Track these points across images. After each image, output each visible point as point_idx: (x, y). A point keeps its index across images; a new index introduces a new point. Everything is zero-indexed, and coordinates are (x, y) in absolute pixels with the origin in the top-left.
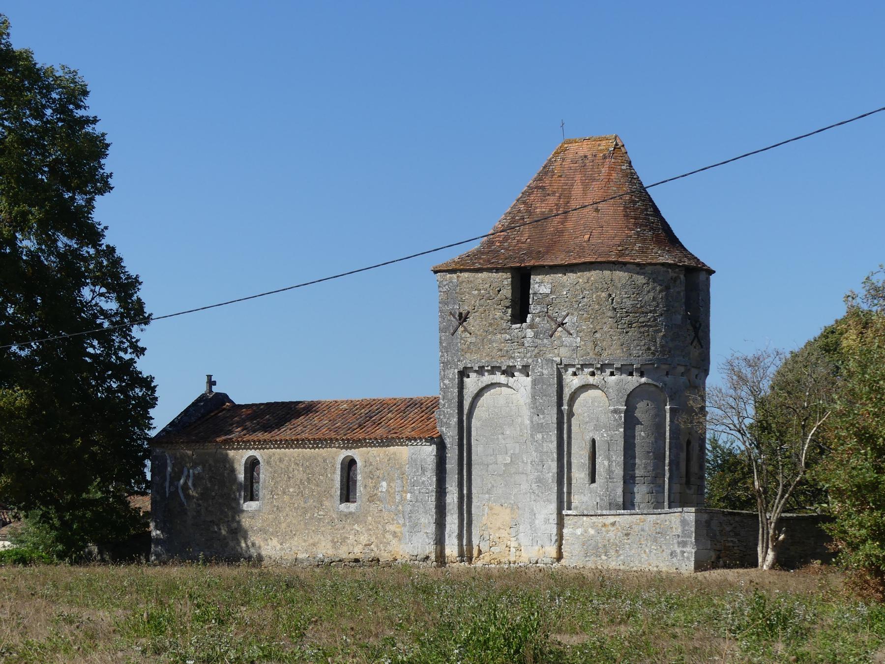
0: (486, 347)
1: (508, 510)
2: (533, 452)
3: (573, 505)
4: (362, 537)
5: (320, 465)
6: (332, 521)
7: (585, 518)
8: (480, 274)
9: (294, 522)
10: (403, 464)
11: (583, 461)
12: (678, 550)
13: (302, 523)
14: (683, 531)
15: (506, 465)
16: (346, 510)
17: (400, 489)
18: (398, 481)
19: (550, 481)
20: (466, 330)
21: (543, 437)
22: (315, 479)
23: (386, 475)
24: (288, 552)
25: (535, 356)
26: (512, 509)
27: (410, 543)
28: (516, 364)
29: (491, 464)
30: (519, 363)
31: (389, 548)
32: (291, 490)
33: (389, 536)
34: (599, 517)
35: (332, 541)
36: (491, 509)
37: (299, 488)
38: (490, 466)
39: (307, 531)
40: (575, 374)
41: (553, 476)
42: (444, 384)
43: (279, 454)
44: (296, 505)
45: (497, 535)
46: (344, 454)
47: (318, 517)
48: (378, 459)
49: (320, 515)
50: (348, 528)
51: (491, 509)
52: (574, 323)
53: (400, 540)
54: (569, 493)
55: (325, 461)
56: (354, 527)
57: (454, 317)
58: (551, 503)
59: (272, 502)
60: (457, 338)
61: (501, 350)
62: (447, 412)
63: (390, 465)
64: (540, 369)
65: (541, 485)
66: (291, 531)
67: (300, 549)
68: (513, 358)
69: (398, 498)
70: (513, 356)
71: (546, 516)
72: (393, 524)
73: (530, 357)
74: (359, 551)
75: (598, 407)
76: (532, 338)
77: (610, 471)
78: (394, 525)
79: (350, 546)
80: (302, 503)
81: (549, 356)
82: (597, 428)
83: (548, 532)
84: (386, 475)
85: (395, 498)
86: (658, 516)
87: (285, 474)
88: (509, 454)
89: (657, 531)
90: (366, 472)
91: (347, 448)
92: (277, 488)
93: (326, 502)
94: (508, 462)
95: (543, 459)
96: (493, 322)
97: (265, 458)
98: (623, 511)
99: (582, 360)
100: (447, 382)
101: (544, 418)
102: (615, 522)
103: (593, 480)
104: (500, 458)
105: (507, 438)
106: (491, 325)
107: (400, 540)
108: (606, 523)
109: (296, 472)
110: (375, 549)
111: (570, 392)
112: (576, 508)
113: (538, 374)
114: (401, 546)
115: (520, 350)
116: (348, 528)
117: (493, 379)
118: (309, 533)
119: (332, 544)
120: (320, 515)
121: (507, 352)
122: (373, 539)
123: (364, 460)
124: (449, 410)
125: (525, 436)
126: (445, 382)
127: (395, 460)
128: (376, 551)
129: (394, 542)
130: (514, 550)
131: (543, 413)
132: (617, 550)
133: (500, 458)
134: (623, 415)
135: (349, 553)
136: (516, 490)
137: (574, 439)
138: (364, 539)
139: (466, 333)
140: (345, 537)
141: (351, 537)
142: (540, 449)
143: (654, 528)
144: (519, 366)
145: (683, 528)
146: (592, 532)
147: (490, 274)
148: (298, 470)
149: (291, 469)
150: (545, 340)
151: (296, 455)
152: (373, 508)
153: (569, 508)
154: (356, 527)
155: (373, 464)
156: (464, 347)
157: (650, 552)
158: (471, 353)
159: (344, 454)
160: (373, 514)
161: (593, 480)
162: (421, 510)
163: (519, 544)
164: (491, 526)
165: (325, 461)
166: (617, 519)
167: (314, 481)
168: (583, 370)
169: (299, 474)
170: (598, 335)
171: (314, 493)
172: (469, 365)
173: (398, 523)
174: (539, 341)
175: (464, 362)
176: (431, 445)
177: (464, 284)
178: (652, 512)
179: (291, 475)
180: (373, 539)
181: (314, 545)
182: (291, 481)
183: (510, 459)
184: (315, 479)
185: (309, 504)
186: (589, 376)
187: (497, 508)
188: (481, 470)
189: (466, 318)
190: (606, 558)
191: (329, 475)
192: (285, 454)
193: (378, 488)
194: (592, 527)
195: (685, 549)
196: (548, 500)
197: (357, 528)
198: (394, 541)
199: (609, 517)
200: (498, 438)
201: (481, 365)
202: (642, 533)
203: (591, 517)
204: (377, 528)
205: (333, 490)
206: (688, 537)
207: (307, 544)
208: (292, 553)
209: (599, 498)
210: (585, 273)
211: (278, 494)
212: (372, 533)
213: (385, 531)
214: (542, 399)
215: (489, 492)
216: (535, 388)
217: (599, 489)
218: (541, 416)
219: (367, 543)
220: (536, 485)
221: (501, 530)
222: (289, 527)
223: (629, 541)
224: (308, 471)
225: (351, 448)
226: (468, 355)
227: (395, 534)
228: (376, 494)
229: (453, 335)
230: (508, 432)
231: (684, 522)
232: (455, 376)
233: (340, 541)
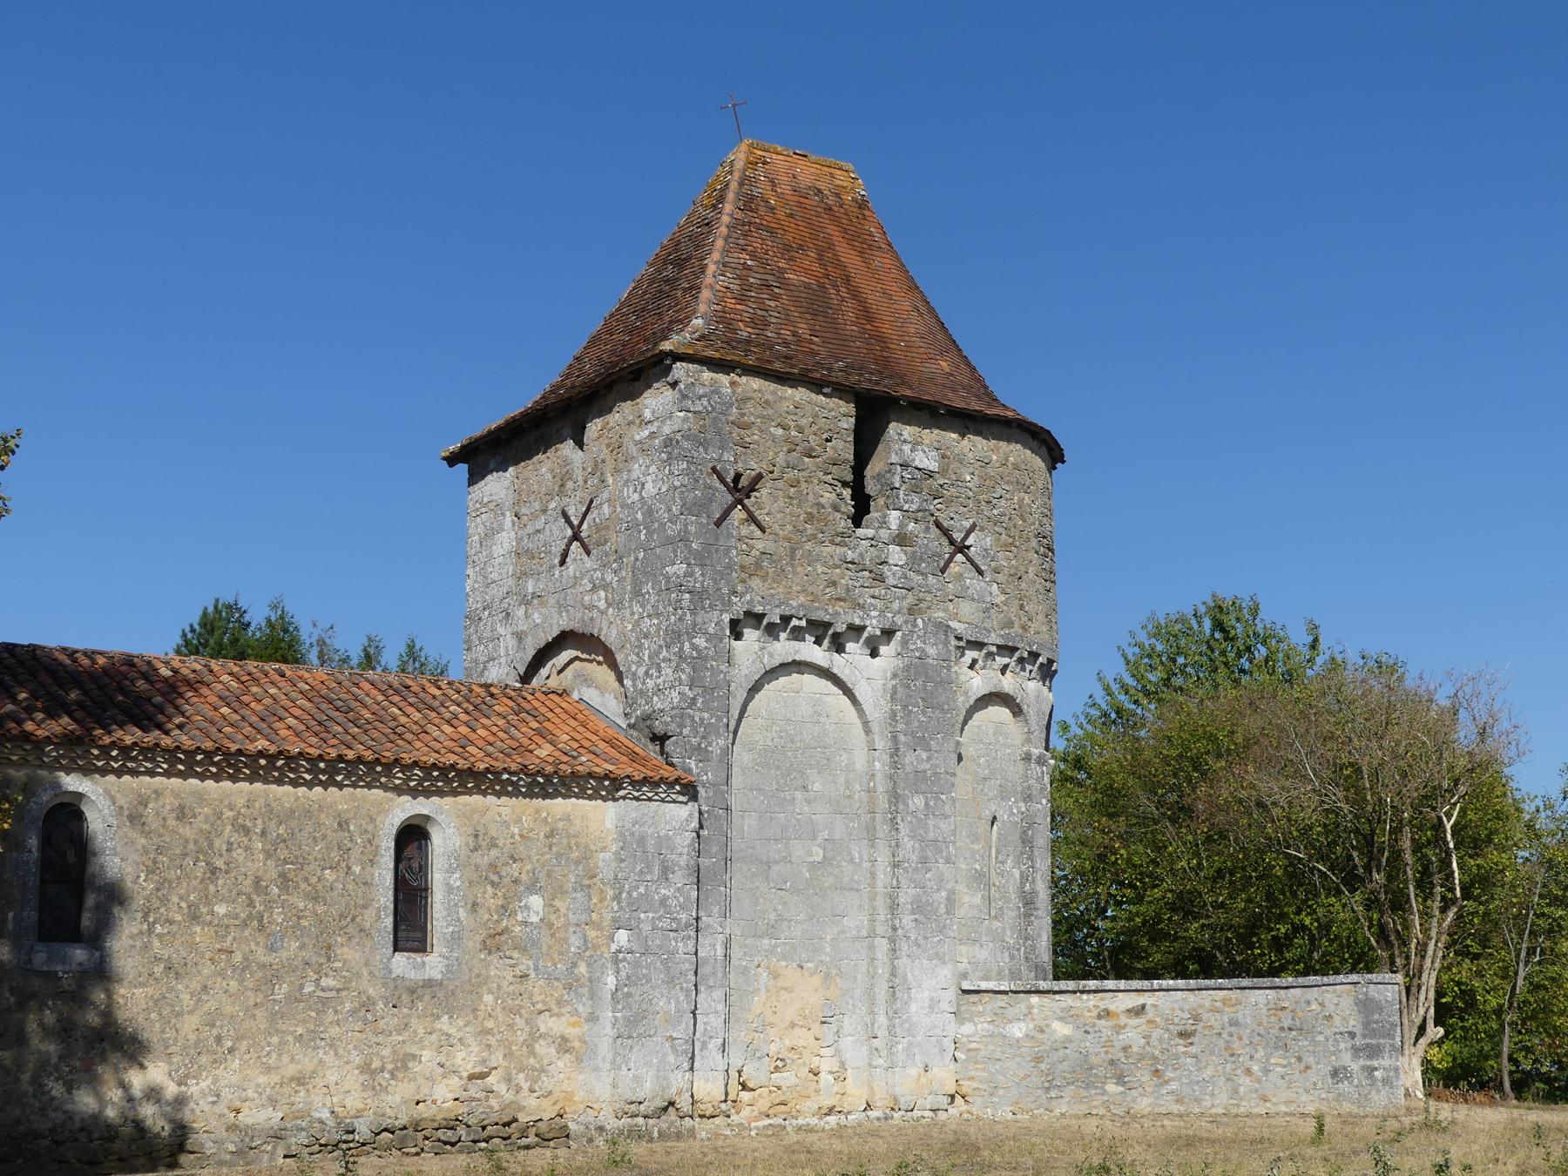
0: (799, 569)
1: (817, 980)
2: (906, 839)
4: (461, 1055)
5: (324, 837)
6: (367, 1005)
7: (1035, 999)
8: (790, 391)
9: (228, 1010)
10: (593, 848)
11: (978, 867)
12: (1355, 1067)
13: (260, 1013)
14: (1366, 1025)
15: (813, 866)
16: (412, 975)
17: (583, 917)
18: (579, 895)
20: (752, 519)
21: (927, 804)
22: (306, 880)
23: (542, 876)
24: (207, 1108)
25: (911, 611)
26: (827, 977)
27: (624, 1068)
28: (868, 623)
29: (777, 863)
30: (874, 622)
31: (546, 1082)
32: (221, 909)
33: (544, 1049)
34: (1085, 997)
35: (365, 1068)
36: (775, 975)
37: (251, 904)
38: (775, 868)
39: (275, 1040)
42: (694, 647)
43: (177, 796)
44: (238, 957)
45: (787, 1042)
46: (404, 808)
47: (323, 994)
48: (516, 831)
49: (323, 990)
50: (418, 1026)
51: (775, 975)
52: (986, 550)
53: (579, 1060)
55: (342, 825)
56: (438, 1025)
57: (722, 480)
58: (944, 963)
59: (146, 947)
60: (730, 535)
61: (834, 584)
62: (702, 719)
63: (554, 849)
64: (919, 644)
65: (922, 918)
66: (219, 1039)
67: (250, 1093)
68: (861, 607)
69: (575, 942)
70: (861, 601)
71: (933, 994)
72: (559, 1015)
74: (451, 1096)
76: (901, 566)
78: (563, 1019)
79: (420, 1080)
80: (260, 951)
82: (1003, 794)
83: (938, 1032)
84: (542, 876)
85: (566, 940)
86: (1282, 992)
87: (198, 860)
88: (819, 840)
89: (1286, 1024)
90: (477, 867)
91: (414, 793)
92: (165, 900)
93: (345, 949)
94: (819, 858)
95: (926, 858)
96: (815, 512)
97: (121, 801)
98: (1171, 982)
99: (1001, 636)
100: (700, 642)
101: (929, 759)
102: (1143, 1007)
104: (798, 850)
105: (815, 800)
106: (810, 518)
107: (579, 1060)
108: (1112, 1008)
109: (238, 854)
110: (501, 1088)
111: (967, 706)
113: (917, 654)
114: (581, 1077)
115: (877, 591)
116: (418, 1026)
117: (797, 652)
118: (283, 1043)
119: (361, 1078)
120: (323, 990)
121: (848, 590)
122: (497, 1058)
123: (470, 831)
124: (706, 715)
125: (856, 798)
126: (697, 641)
127: (569, 836)
128: (500, 1094)
129: (562, 1064)
130: (831, 1078)
132: (1157, 1071)
133: (798, 850)
135: (417, 1103)
136: (835, 930)
137: (390, 848)
138: (466, 1059)
139: (753, 527)
140: (406, 1055)
141: (426, 1055)
142: (921, 831)
143: (1273, 1019)
144: (873, 627)
145: (1366, 1016)
146: (1062, 1030)
147: (813, 396)
148: (247, 848)
149: (218, 843)
150: (930, 577)
151: (241, 802)
152: (499, 970)
154: (444, 1023)
155: (501, 842)
156: (748, 561)
157: (1266, 1071)
158: (764, 578)
159: (404, 808)
160: (499, 987)
162: (658, 977)
163: (843, 1065)
164: (772, 1019)
165: (342, 825)
166: (1148, 999)
167: (303, 885)
169: (253, 862)
171: (304, 923)
172: (759, 609)
173: (575, 1013)
174: (918, 578)
175: (748, 597)
176: (686, 803)
177: (749, 405)
178: (1269, 984)
179: (219, 863)
180: (497, 1058)
181: (300, 1080)
182: (220, 882)
183: (821, 852)
184: (306, 880)
185: (285, 954)
187: (790, 973)
188: (753, 875)
189: (752, 488)
190: (1121, 1089)
191: (357, 869)
192: (201, 797)
193: (513, 914)
194: (1061, 1019)
195: (1375, 1063)
197: (445, 1028)
198: (560, 1064)
199: (1120, 994)
200: (794, 799)
201: (787, 613)
202: (1233, 1029)
203: (1057, 997)
204: (511, 1026)
205: (369, 914)
206: (1384, 1037)
207: (276, 1078)
208: (221, 1108)
210: (1001, 443)
211: (171, 922)
212: (492, 1040)
213: (535, 1036)
214: (924, 713)
215: (772, 931)
216: (908, 687)
217: (1008, 933)
219: (477, 1070)
220: (913, 917)
221: (797, 1030)
222: (213, 1025)
223: (1193, 1050)
224: (282, 854)
225: (428, 793)
226: (755, 583)
227: (564, 1045)
228: (506, 930)
229: (718, 523)
230: (817, 786)
231: (1367, 1007)
232: (723, 629)
233: (390, 1067)
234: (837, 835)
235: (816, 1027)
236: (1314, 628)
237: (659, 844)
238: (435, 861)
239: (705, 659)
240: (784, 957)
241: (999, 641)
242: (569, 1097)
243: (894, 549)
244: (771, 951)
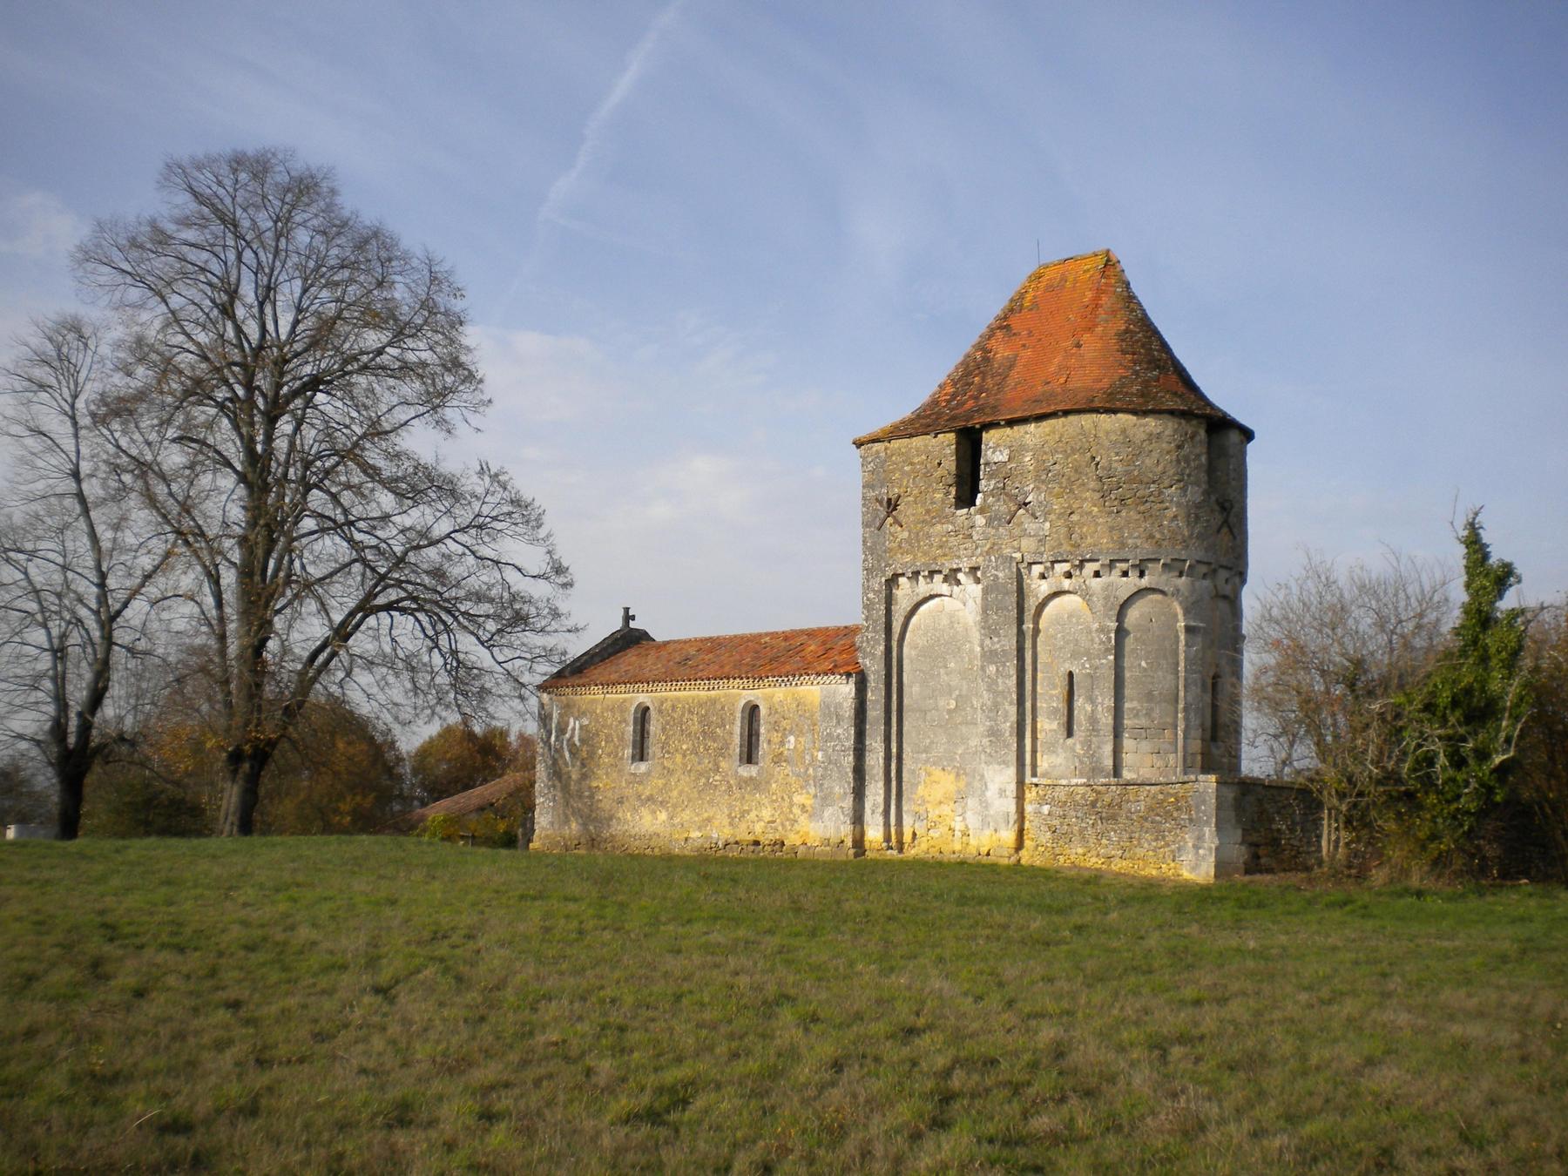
1: (952, 777)
3: (1039, 770)
15: (949, 712)
19: (1007, 734)
26: (958, 775)
38: (929, 714)
40: (1097, 574)
41: (1011, 727)
54: (1034, 752)
57: (881, 504)
73: (981, 554)
75: (1078, 623)
77: (1093, 720)
81: (1007, 551)
82: (1075, 655)
100: (871, 595)
103: (1070, 734)
104: (941, 703)
112: (1044, 775)
131: (998, 635)
134: (1113, 635)
144: (965, 565)
153: (1034, 775)
161: (1070, 734)
168: (1053, 568)
170: (1075, 518)
172: (900, 571)
173: (808, 793)
186: (1063, 579)
187: (937, 773)
196: (1004, 762)
200: (939, 674)
209: (1077, 760)
218: (996, 639)
228: (782, 753)
234: (964, 693)
235: (952, 804)
236: (1219, 531)
237: (836, 708)
238: (1043, 658)
239: (873, 604)
240: (934, 764)
241: (1051, 559)
242: (807, 833)
243: (978, 517)
244: (927, 761)
